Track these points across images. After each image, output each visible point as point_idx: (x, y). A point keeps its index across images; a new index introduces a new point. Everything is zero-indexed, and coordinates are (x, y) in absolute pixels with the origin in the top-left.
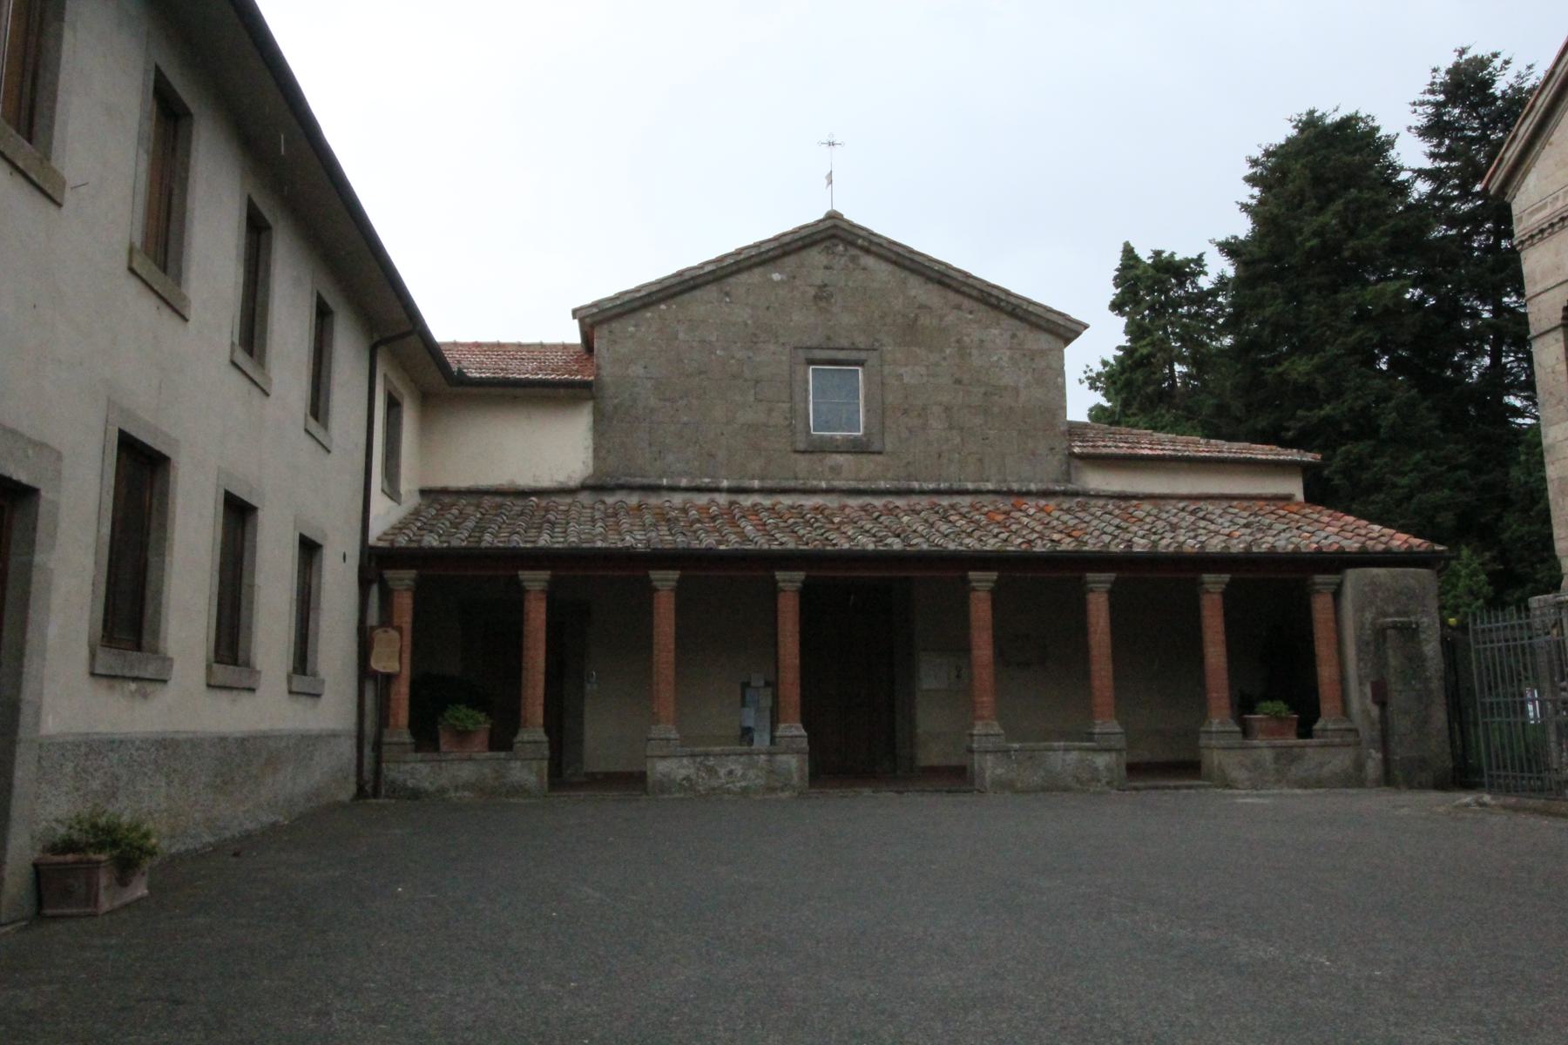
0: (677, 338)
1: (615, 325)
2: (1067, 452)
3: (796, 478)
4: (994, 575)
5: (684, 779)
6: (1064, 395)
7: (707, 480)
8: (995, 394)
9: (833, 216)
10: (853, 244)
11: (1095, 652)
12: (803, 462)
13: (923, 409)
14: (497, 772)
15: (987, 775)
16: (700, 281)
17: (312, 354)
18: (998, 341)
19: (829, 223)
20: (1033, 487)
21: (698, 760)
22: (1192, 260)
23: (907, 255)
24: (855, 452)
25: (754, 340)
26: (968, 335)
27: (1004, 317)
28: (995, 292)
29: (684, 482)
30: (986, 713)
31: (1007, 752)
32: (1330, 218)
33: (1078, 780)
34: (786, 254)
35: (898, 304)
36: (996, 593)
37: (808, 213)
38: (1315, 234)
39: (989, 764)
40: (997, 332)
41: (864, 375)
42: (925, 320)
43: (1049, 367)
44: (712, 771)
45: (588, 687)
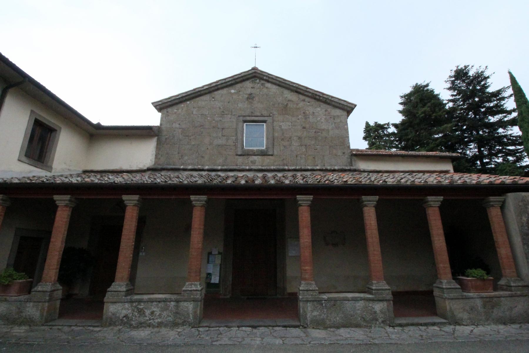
0: (193, 114)
1: (169, 110)
2: (350, 154)
3: (237, 165)
4: (311, 197)
5: (124, 317)
6: (347, 132)
7: (200, 166)
8: (319, 132)
9: (254, 69)
10: (263, 79)
11: (370, 240)
12: (240, 160)
13: (290, 138)
14: (19, 309)
15: (308, 316)
16: (202, 92)
17: (3, 105)
18: (320, 113)
19: (253, 71)
20: (336, 168)
21: (134, 304)
22: (386, 124)
23: (283, 81)
24: (262, 155)
25: (223, 114)
26: (308, 111)
27: (322, 104)
28: (318, 94)
29: (190, 167)
30: (307, 276)
31: (319, 301)
32: (426, 108)
33: (365, 320)
34: (237, 83)
35: (280, 99)
36: (312, 207)
37: (244, 67)
38: (422, 113)
39: (309, 309)
40: (320, 110)
41: (266, 126)
42: (290, 105)
43: (341, 121)
44: (141, 312)
45: (141, 254)
